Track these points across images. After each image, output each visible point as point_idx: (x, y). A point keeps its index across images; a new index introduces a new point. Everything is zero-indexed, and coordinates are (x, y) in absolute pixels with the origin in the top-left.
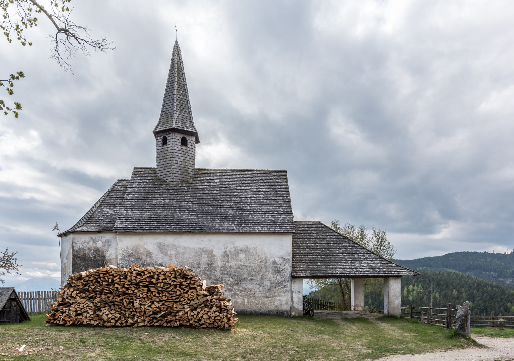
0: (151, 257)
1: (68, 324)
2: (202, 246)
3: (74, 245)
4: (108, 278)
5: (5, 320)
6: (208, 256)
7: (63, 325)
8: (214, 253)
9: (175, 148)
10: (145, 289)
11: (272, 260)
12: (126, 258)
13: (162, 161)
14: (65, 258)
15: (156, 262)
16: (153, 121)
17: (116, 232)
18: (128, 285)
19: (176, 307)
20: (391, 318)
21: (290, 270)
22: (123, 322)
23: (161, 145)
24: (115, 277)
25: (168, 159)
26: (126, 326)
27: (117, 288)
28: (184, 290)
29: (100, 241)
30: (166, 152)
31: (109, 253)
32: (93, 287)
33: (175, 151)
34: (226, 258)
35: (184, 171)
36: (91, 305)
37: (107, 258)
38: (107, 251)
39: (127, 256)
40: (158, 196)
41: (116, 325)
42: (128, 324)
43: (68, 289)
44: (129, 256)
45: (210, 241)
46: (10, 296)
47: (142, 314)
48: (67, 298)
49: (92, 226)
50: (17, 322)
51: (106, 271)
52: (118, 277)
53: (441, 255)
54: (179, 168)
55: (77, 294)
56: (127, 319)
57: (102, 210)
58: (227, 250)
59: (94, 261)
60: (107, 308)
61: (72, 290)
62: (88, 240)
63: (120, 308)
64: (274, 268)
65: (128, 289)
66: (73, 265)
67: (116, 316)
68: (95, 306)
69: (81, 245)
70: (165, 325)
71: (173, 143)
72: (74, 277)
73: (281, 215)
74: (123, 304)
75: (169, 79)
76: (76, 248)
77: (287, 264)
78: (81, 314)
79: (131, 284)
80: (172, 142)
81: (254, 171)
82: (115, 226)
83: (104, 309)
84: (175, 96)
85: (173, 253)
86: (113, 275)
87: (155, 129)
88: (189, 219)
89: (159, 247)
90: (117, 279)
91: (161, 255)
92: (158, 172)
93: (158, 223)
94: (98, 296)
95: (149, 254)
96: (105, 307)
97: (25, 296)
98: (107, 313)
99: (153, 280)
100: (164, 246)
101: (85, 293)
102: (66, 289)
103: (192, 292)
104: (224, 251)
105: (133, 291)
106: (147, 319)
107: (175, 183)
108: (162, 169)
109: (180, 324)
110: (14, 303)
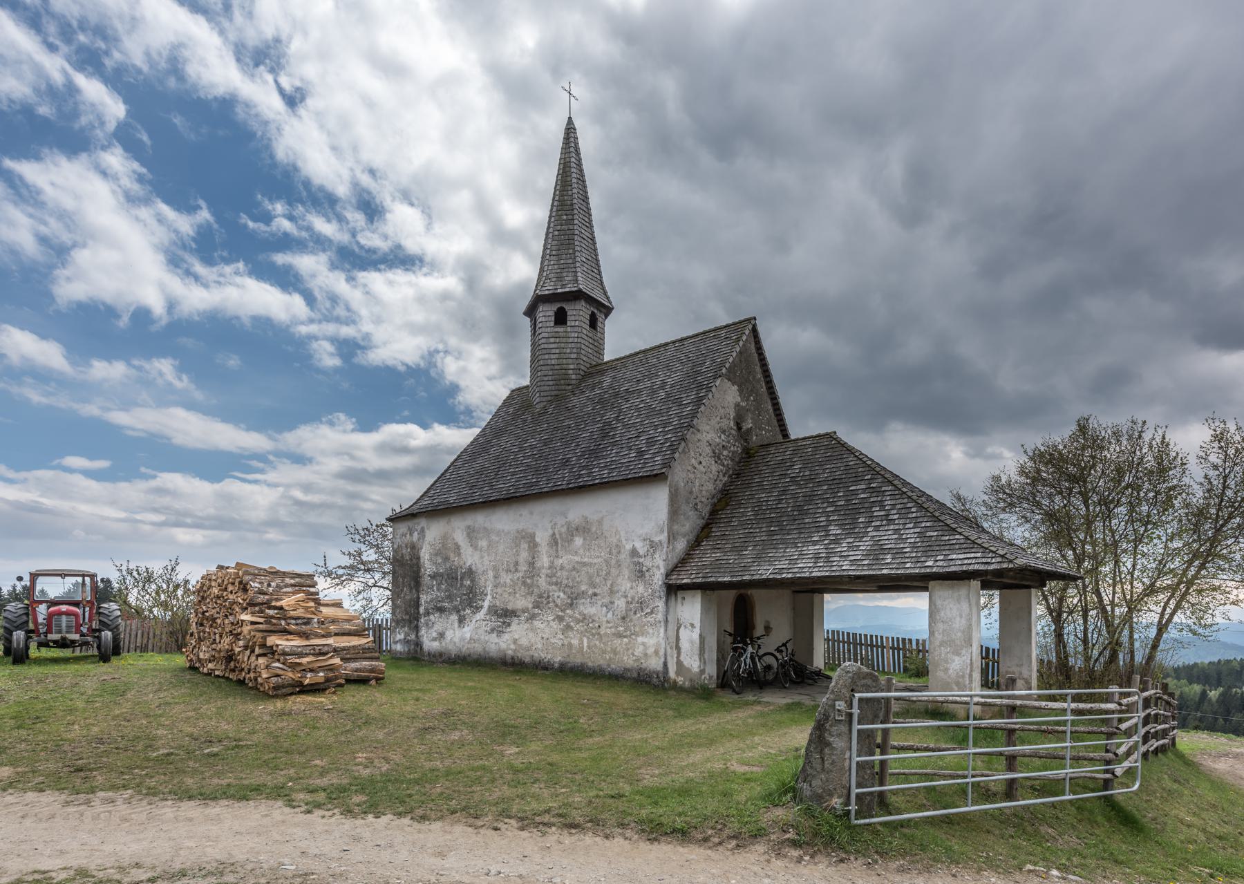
8: (537, 539)
11: (629, 547)
45: (531, 513)
77: (657, 556)
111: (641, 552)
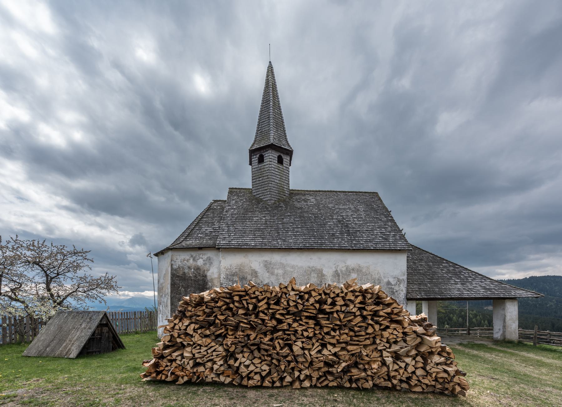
0: (256, 277)
1: (181, 381)
2: (311, 265)
3: (173, 263)
4: (248, 304)
5: (95, 350)
6: (318, 276)
7: (174, 382)
8: (324, 272)
9: (273, 166)
10: (311, 322)
11: (386, 280)
12: (229, 277)
13: (258, 180)
14: (162, 277)
15: (262, 282)
16: (249, 141)
17: (219, 249)
18: (282, 315)
19: (367, 356)
20: (505, 343)
21: (405, 292)
22: (275, 379)
23: (257, 164)
24: (259, 301)
25: (265, 178)
26: (282, 387)
27: (263, 320)
28: (381, 325)
29: (201, 260)
30: (263, 170)
31: (210, 271)
32: (222, 318)
33: (272, 169)
34: (337, 278)
35: (281, 190)
36: (220, 349)
37: (209, 278)
38: (208, 270)
39: (231, 276)
40: (257, 213)
41: (264, 385)
42: (284, 384)
43: (180, 320)
44: (233, 275)
45: (320, 259)
46: (101, 321)
47: (307, 365)
48: (179, 336)
49: (190, 242)
50: (109, 351)
51: (245, 291)
52: (265, 301)
53: (521, 278)
54: (276, 186)
55: (195, 330)
56: (281, 374)
57: (200, 228)
58: (338, 269)
59: (195, 281)
60: (246, 355)
61: (186, 322)
62: (188, 258)
63: (270, 355)
64: (388, 289)
65: (280, 322)
66: (171, 284)
67: (263, 368)
68: (227, 350)
69: (180, 263)
70: (347, 385)
71: (271, 160)
72: (191, 300)
73: (390, 232)
74: (275, 348)
75: (263, 98)
76: (175, 267)
77: (402, 285)
78: (203, 365)
79: (288, 313)
80: (269, 160)
81: (346, 192)
82: (218, 242)
83: (241, 355)
84: (271, 113)
85: (280, 272)
86: (256, 297)
87: (251, 147)
88: (295, 236)
89: (265, 266)
90: (262, 305)
91: (267, 274)
92: (254, 191)
93: (263, 239)
94: (230, 333)
95: (255, 273)
96: (242, 352)
97: (122, 317)
98: (246, 363)
99: (325, 307)
100: (270, 264)
101: (209, 328)
102: (177, 321)
103: (395, 329)
104: (334, 269)
105: (290, 325)
106: (315, 375)
107: (272, 202)
108: (258, 187)
109: (374, 385)
110: (105, 329)
111: (393, 283)
